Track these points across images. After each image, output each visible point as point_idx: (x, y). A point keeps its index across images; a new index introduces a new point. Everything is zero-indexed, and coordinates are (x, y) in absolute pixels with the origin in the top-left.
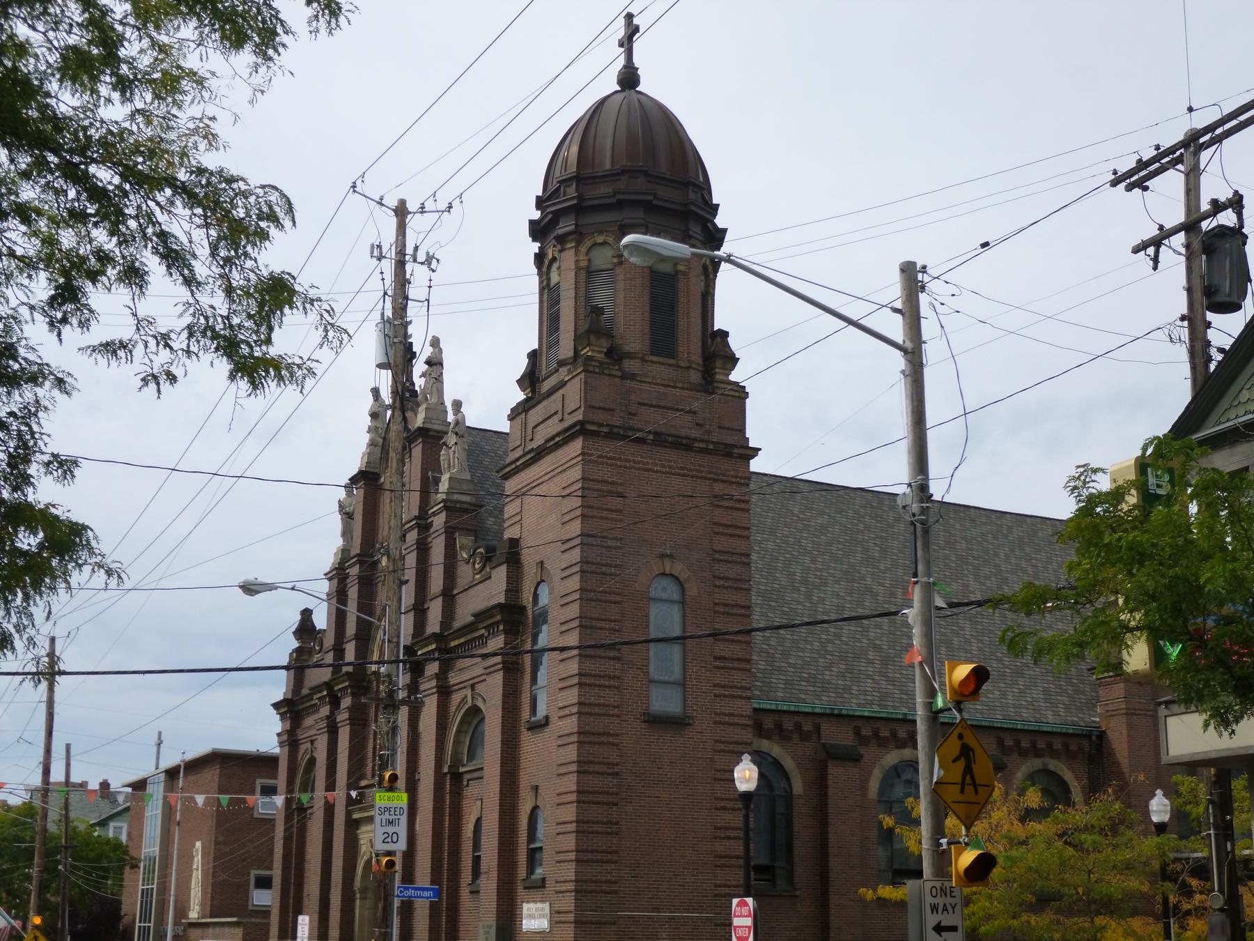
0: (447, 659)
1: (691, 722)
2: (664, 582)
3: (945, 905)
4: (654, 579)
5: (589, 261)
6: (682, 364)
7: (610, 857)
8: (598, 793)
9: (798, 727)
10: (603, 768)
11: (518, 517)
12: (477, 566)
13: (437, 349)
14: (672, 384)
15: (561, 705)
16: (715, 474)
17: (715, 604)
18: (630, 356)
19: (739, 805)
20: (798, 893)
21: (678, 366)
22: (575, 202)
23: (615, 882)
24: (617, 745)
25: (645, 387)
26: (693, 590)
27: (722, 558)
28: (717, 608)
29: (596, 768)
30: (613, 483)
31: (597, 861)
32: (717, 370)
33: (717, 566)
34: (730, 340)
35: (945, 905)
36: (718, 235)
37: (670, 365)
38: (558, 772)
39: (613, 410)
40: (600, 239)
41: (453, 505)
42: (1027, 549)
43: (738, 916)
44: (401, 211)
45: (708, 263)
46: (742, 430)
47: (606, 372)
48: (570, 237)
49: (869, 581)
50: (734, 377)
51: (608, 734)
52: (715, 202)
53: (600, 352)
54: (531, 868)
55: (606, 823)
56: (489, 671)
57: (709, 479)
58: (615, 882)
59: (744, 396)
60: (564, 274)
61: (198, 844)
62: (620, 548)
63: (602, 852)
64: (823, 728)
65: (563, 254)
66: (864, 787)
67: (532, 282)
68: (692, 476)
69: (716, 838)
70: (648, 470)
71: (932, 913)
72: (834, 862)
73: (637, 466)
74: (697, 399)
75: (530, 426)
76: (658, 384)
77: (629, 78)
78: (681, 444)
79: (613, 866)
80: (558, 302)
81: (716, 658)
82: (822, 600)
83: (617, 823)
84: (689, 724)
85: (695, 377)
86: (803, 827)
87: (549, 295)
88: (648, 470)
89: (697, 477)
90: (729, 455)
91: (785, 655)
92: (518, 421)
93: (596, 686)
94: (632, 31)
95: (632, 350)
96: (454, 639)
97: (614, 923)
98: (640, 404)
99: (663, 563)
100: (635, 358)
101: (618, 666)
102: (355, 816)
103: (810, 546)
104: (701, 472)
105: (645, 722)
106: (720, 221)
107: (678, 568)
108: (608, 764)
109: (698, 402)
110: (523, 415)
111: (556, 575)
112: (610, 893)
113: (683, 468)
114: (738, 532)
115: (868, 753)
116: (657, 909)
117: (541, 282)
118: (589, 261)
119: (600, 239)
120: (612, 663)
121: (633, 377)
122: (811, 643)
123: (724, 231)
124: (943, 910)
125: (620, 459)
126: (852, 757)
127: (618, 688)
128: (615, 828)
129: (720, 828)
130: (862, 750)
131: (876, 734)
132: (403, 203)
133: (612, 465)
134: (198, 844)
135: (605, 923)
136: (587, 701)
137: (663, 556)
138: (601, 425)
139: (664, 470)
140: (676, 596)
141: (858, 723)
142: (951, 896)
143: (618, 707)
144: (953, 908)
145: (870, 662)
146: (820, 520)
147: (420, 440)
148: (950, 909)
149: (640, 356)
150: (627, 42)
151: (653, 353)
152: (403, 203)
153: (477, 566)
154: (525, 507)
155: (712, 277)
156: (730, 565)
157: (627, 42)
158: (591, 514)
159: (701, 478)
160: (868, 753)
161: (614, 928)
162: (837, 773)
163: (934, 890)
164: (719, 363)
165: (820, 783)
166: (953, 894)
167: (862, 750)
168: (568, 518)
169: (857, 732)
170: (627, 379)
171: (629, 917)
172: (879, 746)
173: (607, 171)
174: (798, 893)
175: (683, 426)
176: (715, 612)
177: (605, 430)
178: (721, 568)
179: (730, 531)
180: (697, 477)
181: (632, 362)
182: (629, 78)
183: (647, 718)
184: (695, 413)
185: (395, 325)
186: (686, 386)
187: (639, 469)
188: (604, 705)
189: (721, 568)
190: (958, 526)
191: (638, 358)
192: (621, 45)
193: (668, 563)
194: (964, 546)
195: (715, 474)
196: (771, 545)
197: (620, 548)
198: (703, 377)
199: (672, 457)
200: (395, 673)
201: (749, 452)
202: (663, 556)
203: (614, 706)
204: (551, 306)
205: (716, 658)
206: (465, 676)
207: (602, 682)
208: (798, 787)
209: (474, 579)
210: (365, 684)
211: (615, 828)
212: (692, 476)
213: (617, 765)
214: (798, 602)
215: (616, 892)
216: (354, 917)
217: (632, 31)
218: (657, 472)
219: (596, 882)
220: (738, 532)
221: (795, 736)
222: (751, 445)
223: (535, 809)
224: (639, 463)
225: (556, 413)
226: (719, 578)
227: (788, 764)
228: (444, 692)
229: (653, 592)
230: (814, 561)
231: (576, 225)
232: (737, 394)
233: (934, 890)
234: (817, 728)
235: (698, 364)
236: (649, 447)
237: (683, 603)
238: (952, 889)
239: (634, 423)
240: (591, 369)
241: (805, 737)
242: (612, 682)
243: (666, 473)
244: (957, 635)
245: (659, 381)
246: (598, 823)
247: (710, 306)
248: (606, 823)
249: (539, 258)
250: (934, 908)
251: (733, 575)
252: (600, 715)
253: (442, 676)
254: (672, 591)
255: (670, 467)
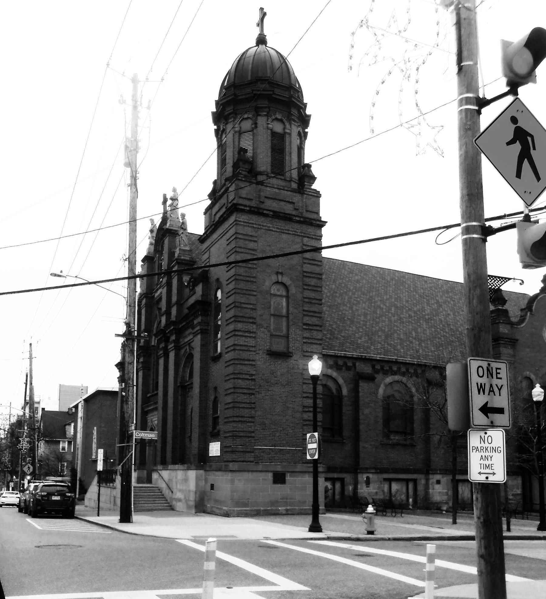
0: (180, 333)
1: (291, 355)
2: (279, 287)
3: (491, 386)
4: (272, 285)
5: (240, 128)
6: (288, 179)
7: (250, 420)
8: (244, 388)
9: (345, 363)
10: (248, 377)
11: (208, 260)
12: (191, 288)
13: (175, 193)
14: (282, 188)
15: (226, 346)
16: (304, 233)
17: (304, 298)
18: (261, 173)
19: (311, 382)
20: (344, 441)
21: (285, 180)
22: (233, 97)
23: (253, 432)
24: (254, 365)
25: (268, 189)
26: (293, 290)
27: (307, 275)
28: (305, 300)
29: (244, 376)
30: (251, 236)
31: (244, 422)
32: (306, 183)
33: (305, 279)
34: (312, 168)
35: (491, 386)
36: (307, 118)
37: (281, 179)
38: (225, 379)
39: (252, 200)
40: (246, 116)
41: (180, 261)
42: (450, 294)
43: (310, 443)
44: (135, 81)
45: (301, 131)
46: (318, 213)
47: (248, 180)
48: (230, 116)
49: (379, 303)
50: (314, 187)
51: (249, 360)
52: (305, 102)
53: (245, 171)
54: (214, 427)
55: (249, 403)
56: (195, 335)
57: (301, 236)
58: (253, 432)
59: (319, 195)
60: (228, 138)
61: (95, 428)
62: (256, 268)
63: (247, 417)
64: (357, 364)
65: (227, 125)
66: (376, 393)
67: (213, 143)
68: (293, 234)
69: (304, 411)
70: (270, 230)
71: (479, 393)
72: (362, 427)
73: (264, 228)
74: (295, 196)
75: (213, 214)
76: (275, 188)
77: (261, 40)
78: (287, 217)
79: (252, 424)
80: (225, 151)
81: (304, 324)
82: (357, 310)
83: (254, 403)
84: (291, 356)
85: (294, 186)
86: (347, 410)
87: (222, 147)
88: (270, 230)
89: (295, 235)
90: (311, 224)
91: (340, 332)
92: (208, 214)
93: (243, 336)
94: (263, 15)
95: (262, 170)
96: (181, 323)
97: (253, 452)
98: (266, 197)
99: (278, 277)
100: (263, 175)
101: (255, 326)
102: (146, 410)
103: (352, 288)
104: (297, 232)
105: (268, 354)
106: (308, 112)
107: (286, 280)
108: (249, 374)
109: (296, 198)
110: (210, 211)
111: (224, 283)
112: (251, 437)
113: (288, 230)
114: (316, 263)
115: (379, 377)
116: (275, 446)
117: (218, 143)
118: (240, 128)
119: (246, 116)
120: (251, 325)
121: (261, 183)
122: (352, 328)
123: (309, 116)
124: (490, 391)
125: (256, 224)
126: (370, 378)
127: (254, 337)
128: (253, 406)
129: (306, 407)
130: (376, 376)
131: (382, 368)
132: (135, 75)
133: (251, 227)
134: (95, 428)
135: (248, 452)
136: (239, 344)
137: (277, 273)
138: (245, 206)
139: (278, 231)
140: (284, 294)
141: (374, 363)
142: (497, 378)
143: (255, 347)
144: (500, 390)
145: (379, 336)
146: (356, 278)
147: (168, 235)
148: (496, 390)
149: (266, 173)
150: (261, 24)
151: (272, 173)
152: (135, 75)
153: (191, 288)
154: (211, 254)
155: (303, 139)
156: (312, 279)
157: (261, 24)
158: (240, 251)
159: (298, 235)
160: (379, 377)
161: (253, 454)
162: (364, 386)
163: (480, 370)
164: (306, 180)
165: (355, 390)
166: (499, 376)
167: (376, 376)
168: (229, 254)
169: (373, 367)
170: (259, 184)
171: (260, 449)
172: (384, 374)
173: (249, 81)
174: (344, 441)
175: (288, 209)
176: (304, 302)
177: (248, 209)
178: (308, 280)
179: (311, 262)
180: (295, 235)
181: (262, 176)
182: (261, 40)
183: (269, 353)
184: (294, 203)
185: (131, 141)
186: (289, 189)
187: (265, 229)
188: (247, 346)
189: (308, 280)
190: (419, 283)
191: (265, 174)
192: (258, 25)
193: (280, 277)
194: (422, 291)
195: (304, 233)
196: (334, 287)
197: (256, 268)
198: (298, 187)
199: (280, 224)
200: (132, 322)
201: (321, 223)
202: (277, 273)
203: (252, 347)
204: (222, 155)
205: (304, 324)
206: (186, 340)
207: (247, 334)
208: (345, 392)
209: (190, 294)
210: (149, 351)
211: (253, 406)
212: (293, 234)
213: (254, 375)
214: (346, 310)
215: (253, 437)
216: (145, 454)
217: (263, 15)
218: (274, 231)
219: (244, 431)
220: (316, 263)
221: (344, 368)
222: (322, 220)
223: (216, 398)
224: (265, 226)
225: (224, 204)
226: (306, 285)
227: (341, 381)
228: (178, 348)
229: (273, 291)
230: (354, 294)
231: (233, 109)
232: (316, 195)
233: (480, 370)
234: (354, 365)
235: (296, 179)
236: (270, 219)
237: (287, 297)
238: (498, 371)
239: (262, 206)
240: (240, 178)
241: (349, 369)
242: (251, 335)
243: (279, 232)
244: (420, 327)
245: (276, 187)
246: (244, 403)
247: (302, 154)
248: (249, 403)
249: (217, 132)
250: (481, 389)
251: (313, 284)
252: (245, 350)
253: (176, 341)
254: (283, 292)
255: (281, 229)
